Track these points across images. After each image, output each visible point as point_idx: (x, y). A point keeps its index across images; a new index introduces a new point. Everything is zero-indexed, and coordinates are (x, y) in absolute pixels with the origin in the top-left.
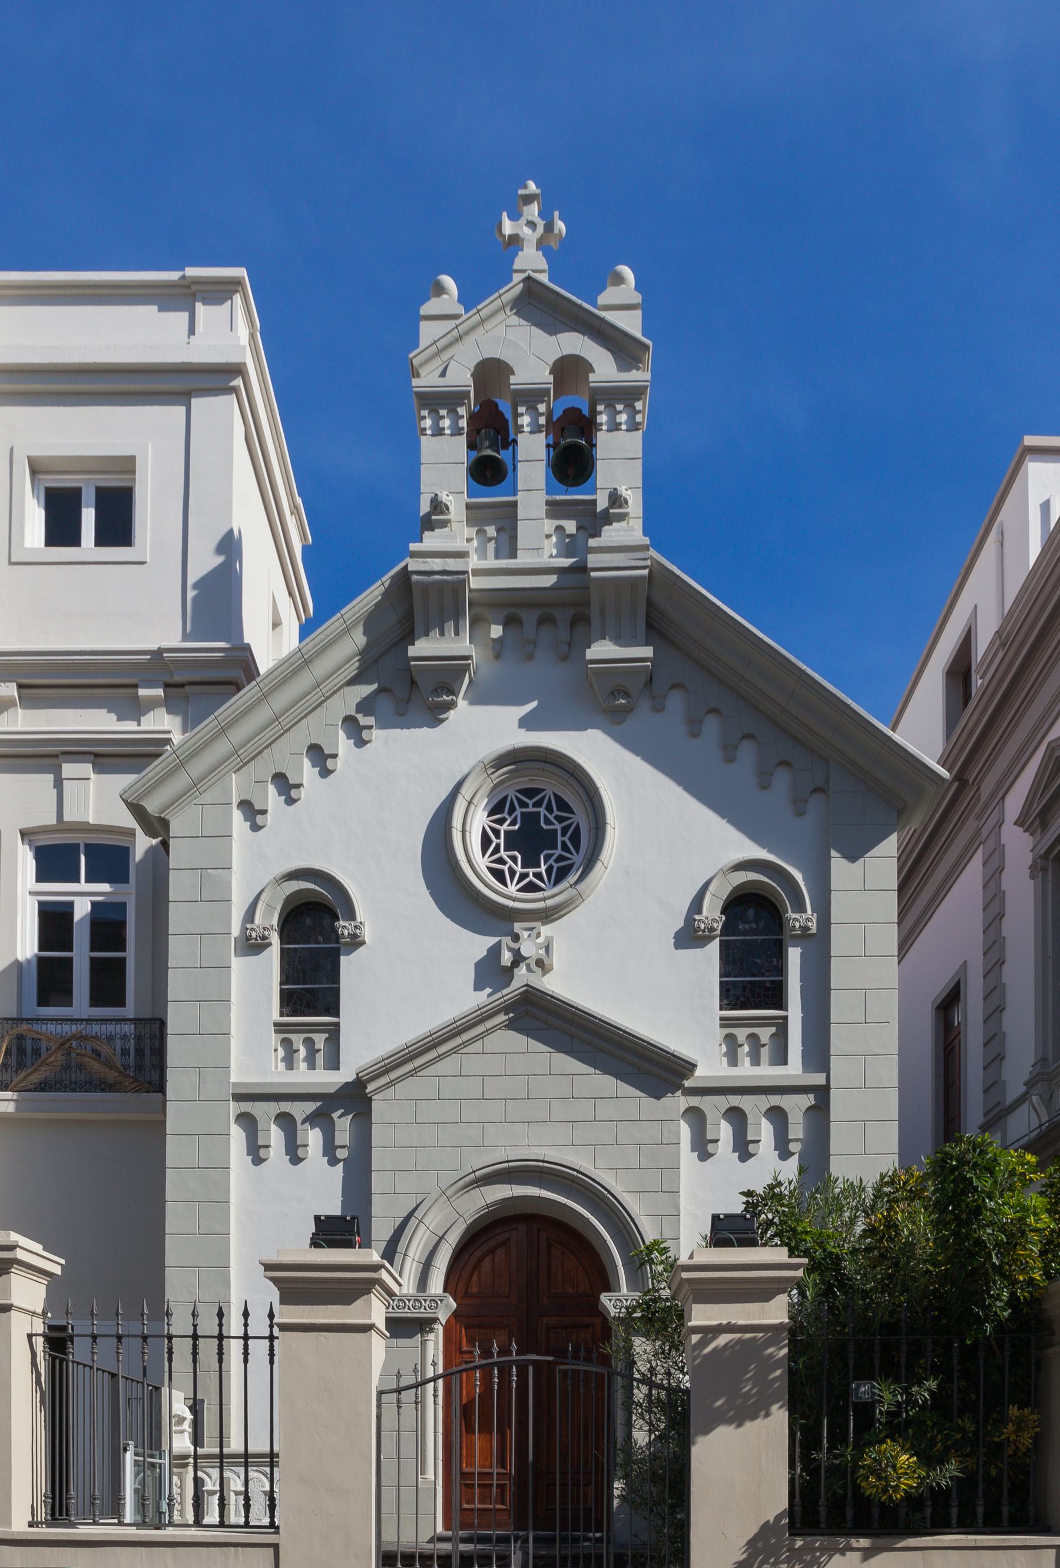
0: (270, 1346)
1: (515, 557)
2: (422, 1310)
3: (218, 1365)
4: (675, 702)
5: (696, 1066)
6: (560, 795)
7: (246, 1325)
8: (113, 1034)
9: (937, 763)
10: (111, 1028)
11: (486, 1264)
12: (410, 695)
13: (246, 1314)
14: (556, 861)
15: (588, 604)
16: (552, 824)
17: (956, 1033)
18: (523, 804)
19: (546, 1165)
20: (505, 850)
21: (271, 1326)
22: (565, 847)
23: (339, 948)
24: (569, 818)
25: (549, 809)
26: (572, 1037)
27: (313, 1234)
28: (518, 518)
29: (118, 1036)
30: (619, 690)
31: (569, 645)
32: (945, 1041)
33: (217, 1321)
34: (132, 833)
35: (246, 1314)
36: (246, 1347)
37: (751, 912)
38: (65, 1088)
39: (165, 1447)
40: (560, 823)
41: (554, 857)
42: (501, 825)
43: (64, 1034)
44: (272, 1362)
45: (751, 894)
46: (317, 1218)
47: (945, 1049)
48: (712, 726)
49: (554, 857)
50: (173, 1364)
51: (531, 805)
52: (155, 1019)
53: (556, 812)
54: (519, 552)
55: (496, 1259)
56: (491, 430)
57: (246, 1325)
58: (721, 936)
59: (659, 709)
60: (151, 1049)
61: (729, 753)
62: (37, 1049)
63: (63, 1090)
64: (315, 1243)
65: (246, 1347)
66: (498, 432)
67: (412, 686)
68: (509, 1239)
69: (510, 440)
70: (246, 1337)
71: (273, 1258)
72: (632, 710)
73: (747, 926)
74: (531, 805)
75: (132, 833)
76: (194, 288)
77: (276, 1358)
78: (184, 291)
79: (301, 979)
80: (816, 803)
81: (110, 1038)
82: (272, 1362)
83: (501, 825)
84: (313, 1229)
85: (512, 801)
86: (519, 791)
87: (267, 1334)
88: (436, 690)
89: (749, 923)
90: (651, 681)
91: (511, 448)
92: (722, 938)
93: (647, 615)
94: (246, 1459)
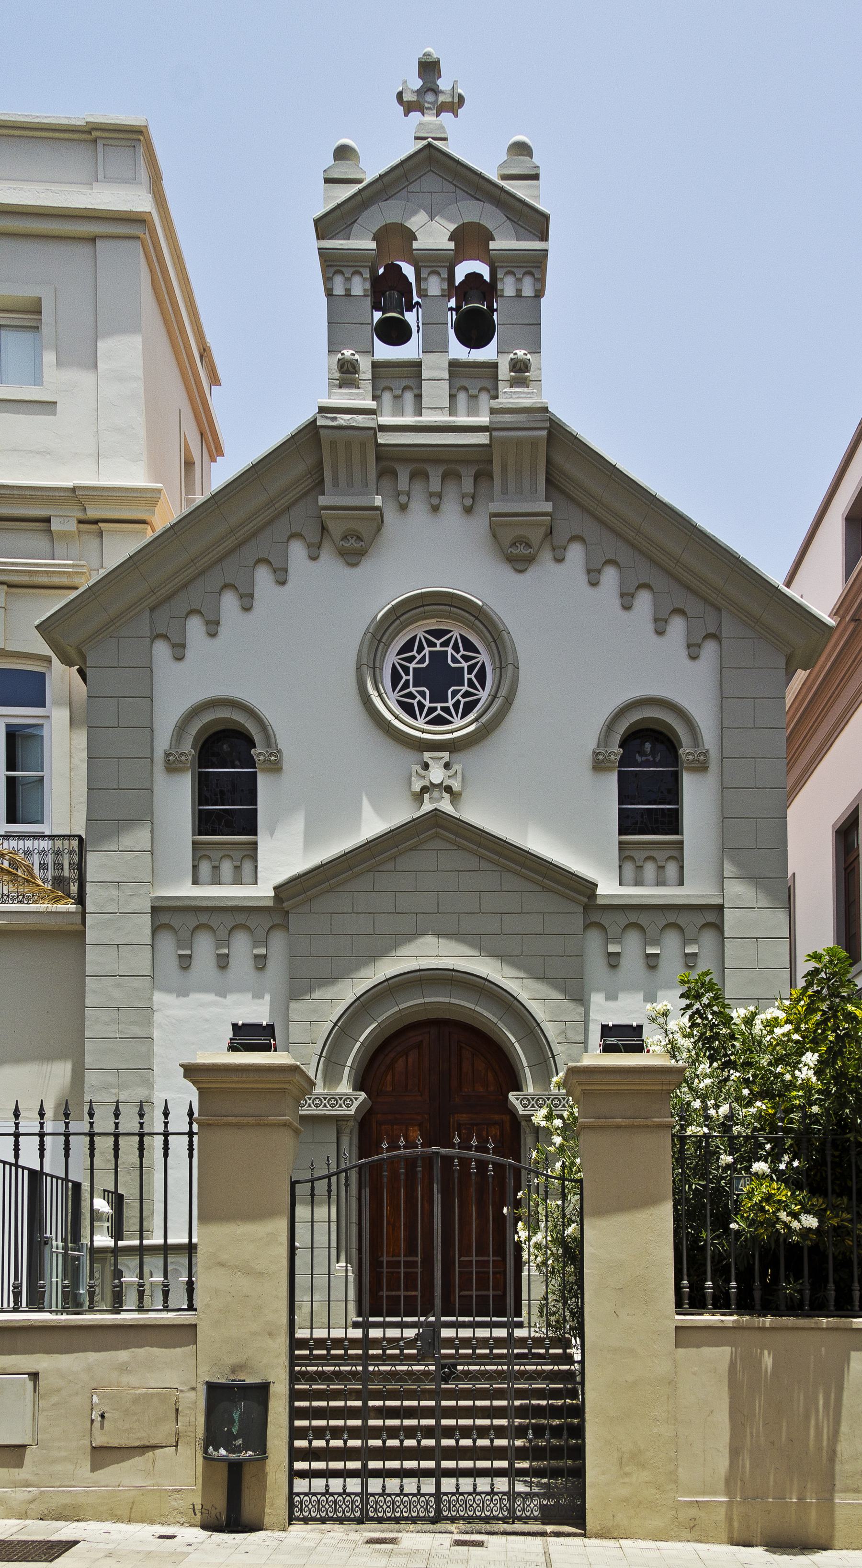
0: (164, 1141)
1: (421, 415)
2: (321, 1108)
3: (188, 1160)
4: (575, 553)
5: (597, 885)
6: (466, 635)
7: (166, 1124)
8: (31, 849)
9: (829, 616)
10: (29, 843)
11: (401, 1063)
12: (321, 540)
13: (166, 1114)
14: (463, 696)
15: (490, 462)
16: (460, 662)
17: (855, 855)
18: (431, 644)
19: (422, 973)
20: (414, 686)
21: (191, 1124)
22: (471, 684)
23: (256, 772)
24: (399, 664)
25: (456, 648)
26: (480, 857)
27: (231, 1039)
28: (423, 378)
29: (36, 851)
30: (523, 542)
31: (473, 498)
32: (845, 861)
33: (188, 1120)
34: (48, 660)
35: (166, 1114)
36: (166, 1143)
37: (648, 746)
38: (29, 898)
39: (86, 1241)
40: (466, 662)
41: (461, 693)
42: (410, 663)
43: (26, 849)
44: (67, 1155)
45: (647, 730)
46: (235, 1026)
47: (846, 869)
48: (610, 576)
49: (461, 693)
50: (95, 1159)
51: (438, 645)
52: (74, 836)
53: (462, 652)
54: (423, 410)
55: (410, 1060)
56: (396, 293)
57: (166, 1124)
58: (619, 767)
59: (559, 560)
60: (70, 864)
61: (627, 601)
62: (44, 864)
63: (26, 902)
64: (233, 1048)
65: (166, 1143)
66: (403, 295)
67: (322, 532)
68: (422, 1041)
69: (414, 302)
70: (166, 1135)
71: (185, 1062)
72: (534, 559)
73: (644, 758)
74: (438, 645)
75: (48, 660)
76: (95, 134)
77: (47, 1153)
78: (84, 136)
79: (219, 800)
80: (710, 649)
81: (28, 853)
82: (67, 1155)
83: (410, 663)
84: (230, 1034)
85: (420, 640)
86: (426, 632)
87: (187, 1130)
88: (346, 537)
89: (646, 755)
90: (551, 533)
91: (415, 310)
92: (620, 769)
93: (547, 473)
94: (166, 1249)
